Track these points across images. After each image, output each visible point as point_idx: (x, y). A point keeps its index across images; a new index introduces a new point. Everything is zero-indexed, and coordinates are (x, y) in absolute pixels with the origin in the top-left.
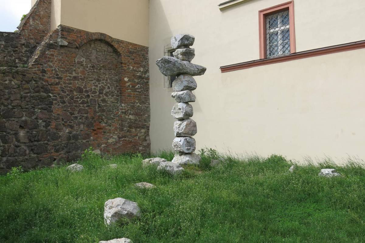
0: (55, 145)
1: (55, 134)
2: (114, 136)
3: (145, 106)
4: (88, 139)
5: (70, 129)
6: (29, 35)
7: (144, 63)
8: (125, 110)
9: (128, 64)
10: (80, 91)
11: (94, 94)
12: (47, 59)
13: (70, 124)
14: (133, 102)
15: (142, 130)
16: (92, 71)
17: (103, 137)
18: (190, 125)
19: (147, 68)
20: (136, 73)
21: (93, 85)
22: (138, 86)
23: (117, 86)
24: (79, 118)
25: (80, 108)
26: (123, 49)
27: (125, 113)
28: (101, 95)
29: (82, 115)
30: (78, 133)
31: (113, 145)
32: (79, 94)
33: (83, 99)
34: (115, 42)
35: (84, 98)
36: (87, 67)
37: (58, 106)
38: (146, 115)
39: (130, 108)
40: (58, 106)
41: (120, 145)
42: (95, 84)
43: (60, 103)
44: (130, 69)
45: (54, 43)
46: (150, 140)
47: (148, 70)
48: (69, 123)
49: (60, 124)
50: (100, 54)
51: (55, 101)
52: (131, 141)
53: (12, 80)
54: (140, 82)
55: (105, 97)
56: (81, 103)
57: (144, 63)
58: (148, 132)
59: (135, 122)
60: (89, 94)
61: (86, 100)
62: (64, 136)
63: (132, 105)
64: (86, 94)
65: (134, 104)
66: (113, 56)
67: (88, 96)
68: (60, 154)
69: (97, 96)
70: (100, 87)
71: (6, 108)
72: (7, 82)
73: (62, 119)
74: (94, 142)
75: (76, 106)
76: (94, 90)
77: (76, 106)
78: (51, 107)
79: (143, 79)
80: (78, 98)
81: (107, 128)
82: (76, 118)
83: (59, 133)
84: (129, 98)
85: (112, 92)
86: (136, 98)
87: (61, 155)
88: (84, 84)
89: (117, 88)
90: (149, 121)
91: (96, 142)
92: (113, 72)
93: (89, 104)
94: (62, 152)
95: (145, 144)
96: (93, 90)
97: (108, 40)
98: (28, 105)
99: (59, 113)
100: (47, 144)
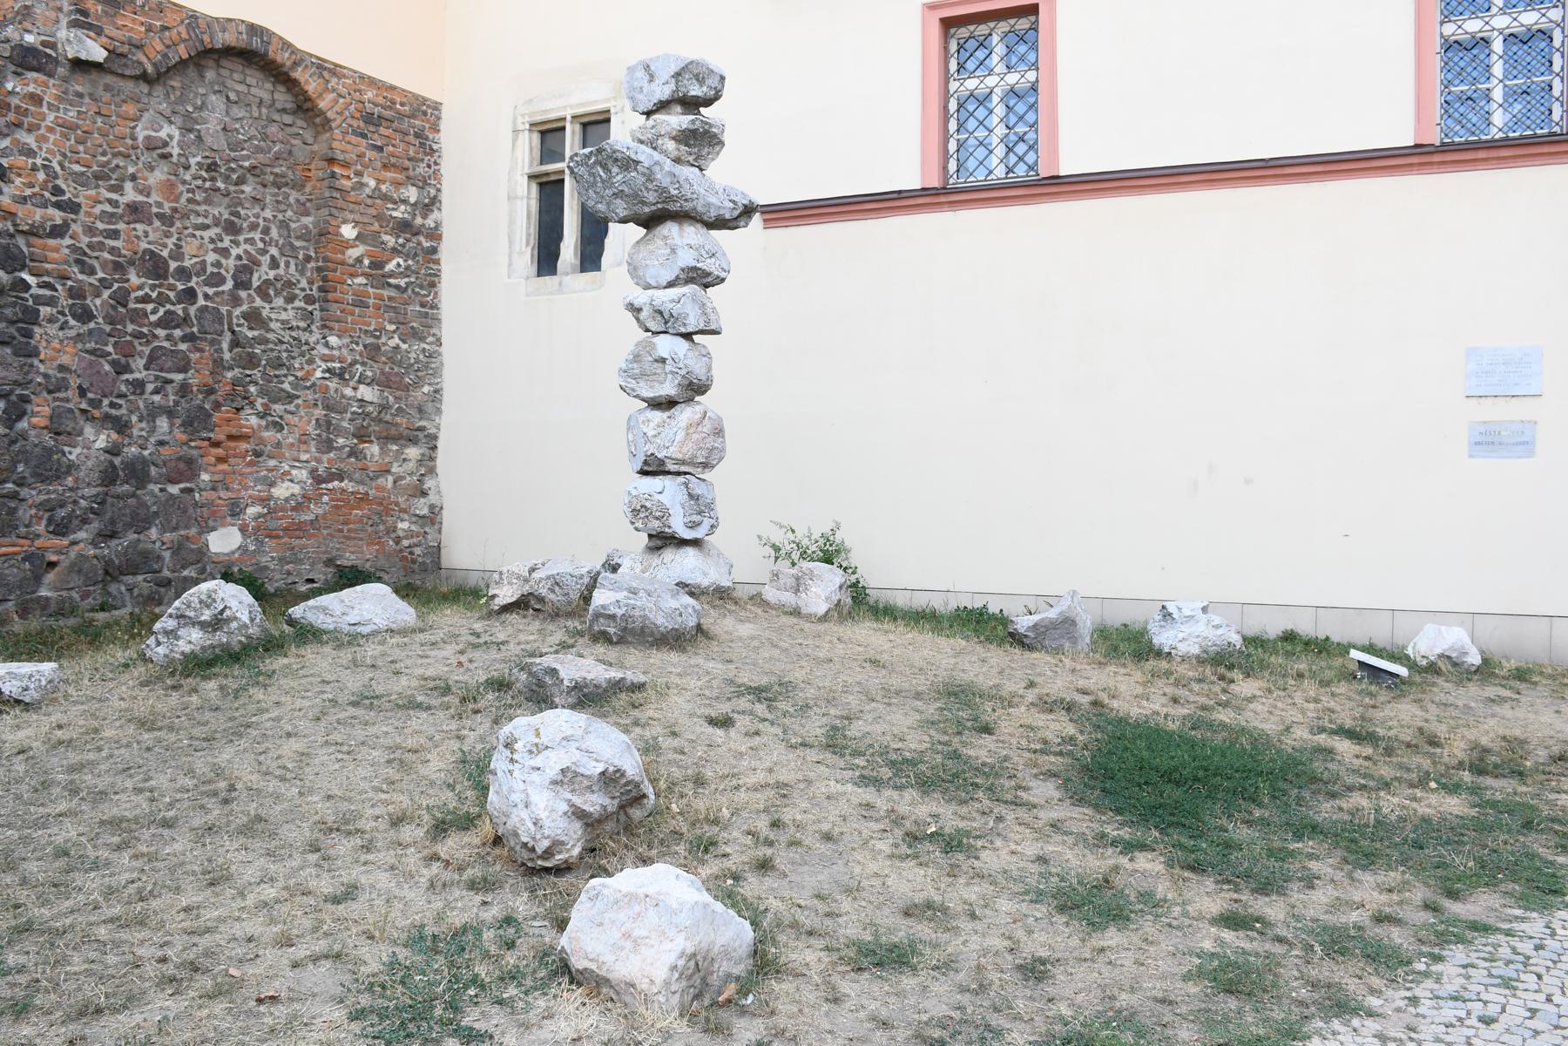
0: (48, 501)
1: (49, 452)
2: (294, 472)
4: (188, 481)
5: (114, 436)
7: (421, 169)
8: (340, 362)
10: (155, 267)
11: (212, 285)
12: (11, 117)
13: (114, 412)
14: (375, 330)
15: (407, 451)
17: (251, 473)
18: (700, 429)
19: (433, 192)
20: (390, 206)
21: (212, 246)
22: (394, 262)
23: (308, 259)
24: (150, 387)
25: (156, 344)
26: (341, 100)
27: (341, 376)
28: (243, 294)
29: (164, 375)
30: (146, 453)
31: (294, 509)
32: (151, 282)
34: (306, 67)
35: (174, 304)
36: (187, 168)
37: (62, 328)
38: (426, 389)
39: (361, 355)
40: (62, 328)
41: (320, 511)
42: (220, 245)
43: (69, 318)
45: (43, 43)
48: (108, 409)
49: (71, 411)
50: (240, 115)
51: (48, 309)
52: (367, 494)
54: (403, 246)
55: (258, 302)
56: (159, 324)
57: (421, 169)
58: (432, 459)
59: (383, 415)
60: (192, 284)
62: (90, 464)
63: (369, 340)
64: (180, 287)
65: (378, 338)
66: (295, 130)
67: (190, 295)
68: (74, 543)
69: (226, 297)
70: (239, 258)
73: (80, 387)
74: (213, 495)
75: (138, 335)
76: (215, 270)
77: (138, 335)
78: (29, 335)
79: (416, 234)
80: (145, 299)
81: (266, 434)
82: (139, 386)
83: (67, 449)
84: (357, 310)
85: (289, 284)
86: (386, 315)
87: (76, 548)
88: (170, 242)
89: (309, 266)
90: (439, 411)
91: (223, 494)
92: (294, 196)
94: (82, 535)
95: (421, 505)
96: (210, 269)
99: (65, 359)
100: (14, 496)
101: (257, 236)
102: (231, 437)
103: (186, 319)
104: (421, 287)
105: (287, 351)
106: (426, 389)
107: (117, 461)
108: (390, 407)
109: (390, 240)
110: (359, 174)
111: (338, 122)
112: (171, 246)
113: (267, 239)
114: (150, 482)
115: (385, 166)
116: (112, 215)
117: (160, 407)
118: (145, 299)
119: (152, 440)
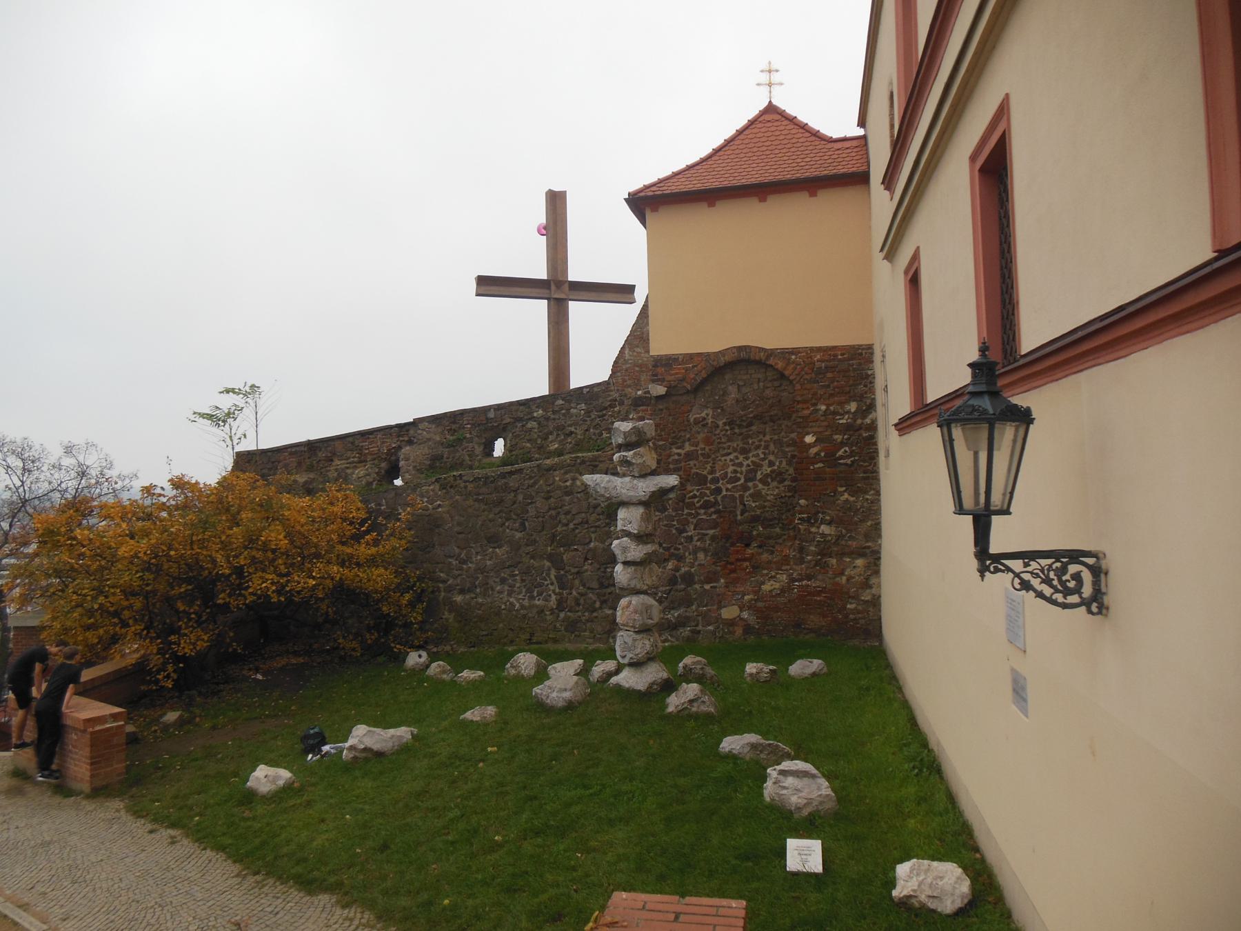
2: (778, 576)
3: (867, 499)
4: (715, 582)
5: (676, 562)
6: (624, 381)
9: (814, 401)
13: (676, 552)
16: (729, 432)
19: (868, 402)
20: (838, 417)
21: (731, 463)
22: (843, 450)
28: (750, 484)
30: (693, 570)
33: (705, 498)
38: (869, 523)
42: (736, 461)
44: (821, 412)
45: (645, 393)
46: (879, 586)
47: (871, 404)
53: (577, 479)
54: (849, 439)
55: (760, 486)
56: (701, 507)
60: (720, 485)
61: (712, 499)
66: (783, 388)
67: (718, 490)
70: (748, 465)
71: (564, 528)
72: (568, 484)
75: (690, 514)
79: (858, 430)
80: (695, 497)
82: (690, 539)
84: (817, 483)
85: (781, 473)
90: (880, 536)
92: (786, 422)
93: (721, 507)
97: (757, 358)
98: (599, 520)
101: (760, 452)
102: (738, 560)
103: (716, 503)
104: (864, 461)
105: (778, 510)
106: (869, 523)
107: (677, 574)
108: (844, 536)
109: (838, 438)
110: (815, 404)
111: (798, 379)
112: (709, 468)
113: (767, 451)
114: (695, 584)
115: (831, 395)
116: (677, 460)
117: (699, 548)
118: (695, 497)
119: (696, 563)
